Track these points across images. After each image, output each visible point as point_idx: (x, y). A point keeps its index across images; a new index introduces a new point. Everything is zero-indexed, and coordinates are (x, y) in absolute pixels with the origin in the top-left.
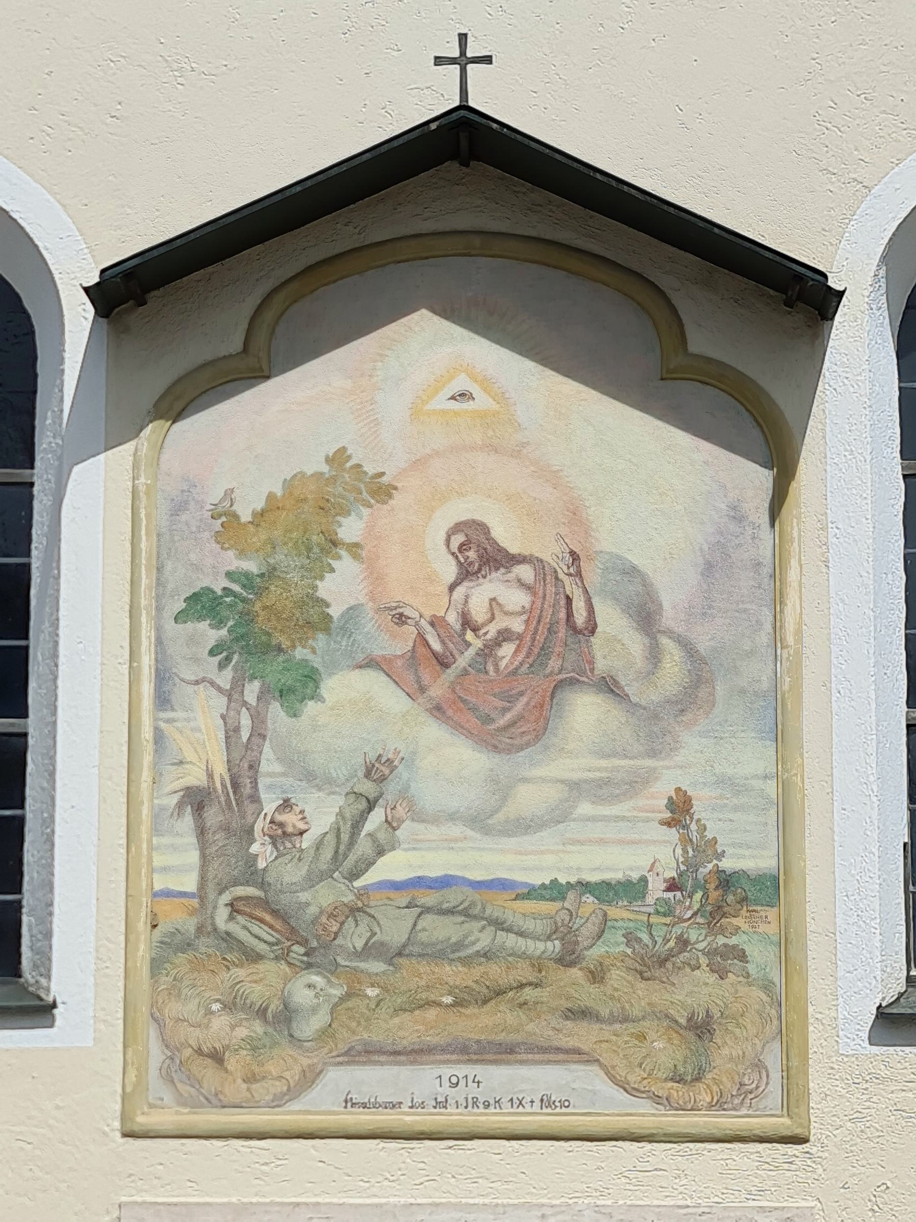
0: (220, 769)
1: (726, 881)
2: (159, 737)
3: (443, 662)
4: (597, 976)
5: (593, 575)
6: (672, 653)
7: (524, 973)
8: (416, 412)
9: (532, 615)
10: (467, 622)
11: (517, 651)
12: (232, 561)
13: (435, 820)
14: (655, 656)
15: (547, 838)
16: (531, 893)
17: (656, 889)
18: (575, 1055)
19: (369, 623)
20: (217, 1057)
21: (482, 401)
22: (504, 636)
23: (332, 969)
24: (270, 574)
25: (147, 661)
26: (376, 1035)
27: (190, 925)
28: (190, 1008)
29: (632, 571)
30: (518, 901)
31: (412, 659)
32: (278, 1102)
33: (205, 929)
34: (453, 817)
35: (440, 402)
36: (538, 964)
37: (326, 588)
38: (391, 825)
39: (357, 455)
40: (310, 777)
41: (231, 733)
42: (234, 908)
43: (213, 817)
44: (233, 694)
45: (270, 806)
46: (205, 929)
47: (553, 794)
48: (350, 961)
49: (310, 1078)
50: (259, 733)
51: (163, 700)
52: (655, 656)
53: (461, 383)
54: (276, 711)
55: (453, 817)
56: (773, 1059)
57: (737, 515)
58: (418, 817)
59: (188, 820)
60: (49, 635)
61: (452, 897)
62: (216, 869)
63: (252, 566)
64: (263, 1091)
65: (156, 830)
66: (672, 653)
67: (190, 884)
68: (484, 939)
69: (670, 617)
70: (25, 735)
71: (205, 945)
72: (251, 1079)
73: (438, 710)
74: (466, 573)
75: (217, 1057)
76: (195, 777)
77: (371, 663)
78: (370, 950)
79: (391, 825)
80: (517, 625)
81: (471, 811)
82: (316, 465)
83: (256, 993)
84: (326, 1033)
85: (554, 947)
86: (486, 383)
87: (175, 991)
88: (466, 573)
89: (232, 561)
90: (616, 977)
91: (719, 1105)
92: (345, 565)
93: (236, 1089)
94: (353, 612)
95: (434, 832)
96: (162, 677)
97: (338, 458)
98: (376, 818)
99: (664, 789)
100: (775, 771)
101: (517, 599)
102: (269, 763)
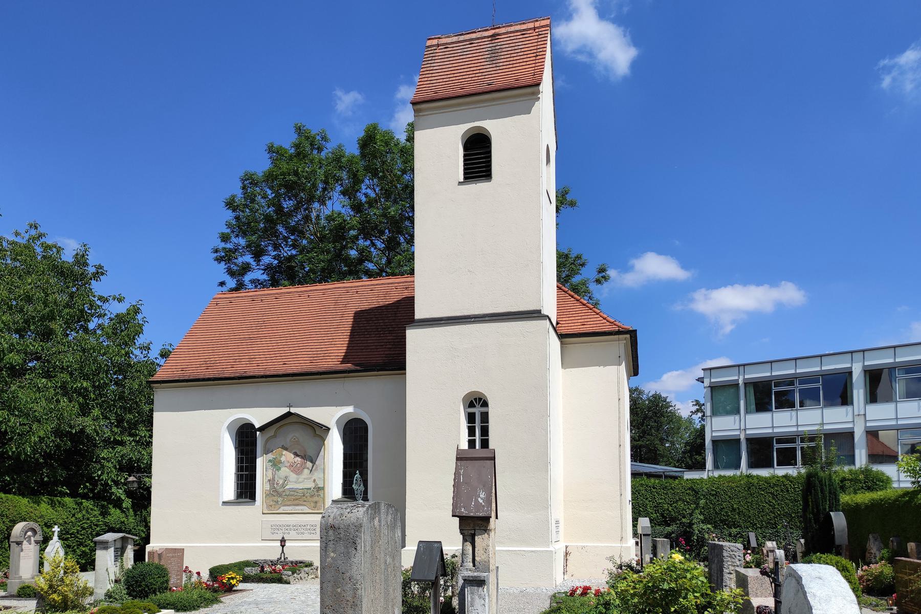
0: (272, 477)
1: (319, 488)
2: (266, 474)
16: (301, 489)
17: (312, 488)
18: (305, 505)
19: (286, 462)
22: (298, 463)
25: (264, 467)
29: (310, 457)
30: (317, 463)
32: (277, 510)
34: (293, 482)
38: (287, 483)
39: (285, 445)
43: (271, 482)
44: (273, 470)
47: (303, 479)
48: (574, 292)
49: (280, 508)
51: (266, 471)
55: (293, 482)
56: (323, 505)
59: (268, 483)
61: (293, 490)
62: (271, 488)
71: (270, 495)
76: (269, 479)
79: (287, 483)
80: (299, 462)
81: (881, 497)
83: (275, 500)
84: (281, 503)
86: (296, 437)
91: (317, 510)
93: (273, 509)
95: (291, 483)
96: (266, 468)
99: (313, 479)
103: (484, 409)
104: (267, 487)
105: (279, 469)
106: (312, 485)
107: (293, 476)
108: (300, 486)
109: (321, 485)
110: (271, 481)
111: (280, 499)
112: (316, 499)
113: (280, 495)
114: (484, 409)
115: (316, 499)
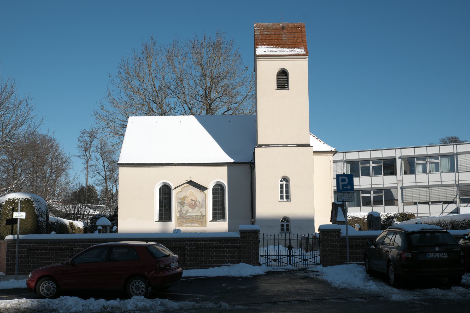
1: (203, 215)
2: (177, 209)
3: (190, 205)
4: (197, 219)
5: (197, 201)
6: (201, 205)
7: (194, 219)
8: (189, 193)
9: (194, 203)
10: (191, 203)
11: (141, 282)
12: (180, 201)
13: (190, 212)
14: (200, 205)
15: (195, 213)
16: (194, 216)
17: (200, 216)
20: (180, 223)
21: (192, 193)
23: (185, 220)
24: (182, 201)
26: (187, 222)
27: (179, 217)
28: (179, 221)
29: (199, 201)
31: (189, 205)
33: (179, 218)
35: (190, 193)
36: (194, 219)
37: (185, 202)
38: (188, 213)
40: (184, 211)
41: (180, 208)
42: (181, 217)
43: (180, 212)
44: (181, 207)
45: (182, 212)
46: (179, 218)
49: (184, 224)
50: (182, 209)
51: (177, 207)
52: (200, 205)
53: (191, 192)
54: (183, 208)
57: (204, 198)
58: (189, 212)
60: (56, 217)
63: (181, 201)
64: (182, 225)
65: (177, 213)
66: (201, 205)
67: (179, 215)
68: (192, 218)
69: (201, 203)
70: (333, 162)
72: (181, 224)
73: (190, 207)
74: (191, 201)
75: (180, 223)
76: (179, 211)
77: (187, 205)
78: (187, 218)
79: (188, 213)
82: (184, 196)
84: (185, 222)
85: (195, 218)
87: (178, 220)
88: (191, 201)
89: (180, 201)
90: (198, 220)
92: (186, 201)
94: (186, 203)
96: (177, 206)
97: (185, 196)
98: (187, 213)
99: (200, 211)
100: (261, 248)
101: (194, 202)
102: (182, 210)
103: (287, 223)
104: (178, 215)
105: (184, 206)
106: (200, 214)
107: (190, 210)
108: (194, 214)
109: (204, 214)
110: (180, 212)
111: (184, 220)
112: (202, 220)
113: (184, 218)
114: (287, 223)
115: (202, 220)
